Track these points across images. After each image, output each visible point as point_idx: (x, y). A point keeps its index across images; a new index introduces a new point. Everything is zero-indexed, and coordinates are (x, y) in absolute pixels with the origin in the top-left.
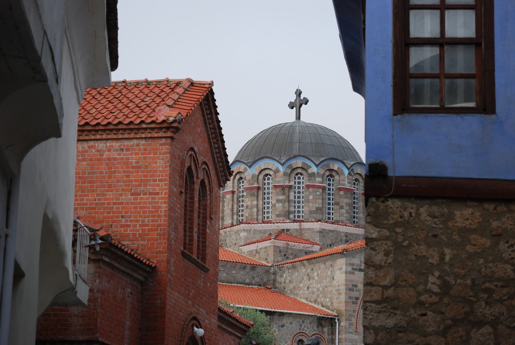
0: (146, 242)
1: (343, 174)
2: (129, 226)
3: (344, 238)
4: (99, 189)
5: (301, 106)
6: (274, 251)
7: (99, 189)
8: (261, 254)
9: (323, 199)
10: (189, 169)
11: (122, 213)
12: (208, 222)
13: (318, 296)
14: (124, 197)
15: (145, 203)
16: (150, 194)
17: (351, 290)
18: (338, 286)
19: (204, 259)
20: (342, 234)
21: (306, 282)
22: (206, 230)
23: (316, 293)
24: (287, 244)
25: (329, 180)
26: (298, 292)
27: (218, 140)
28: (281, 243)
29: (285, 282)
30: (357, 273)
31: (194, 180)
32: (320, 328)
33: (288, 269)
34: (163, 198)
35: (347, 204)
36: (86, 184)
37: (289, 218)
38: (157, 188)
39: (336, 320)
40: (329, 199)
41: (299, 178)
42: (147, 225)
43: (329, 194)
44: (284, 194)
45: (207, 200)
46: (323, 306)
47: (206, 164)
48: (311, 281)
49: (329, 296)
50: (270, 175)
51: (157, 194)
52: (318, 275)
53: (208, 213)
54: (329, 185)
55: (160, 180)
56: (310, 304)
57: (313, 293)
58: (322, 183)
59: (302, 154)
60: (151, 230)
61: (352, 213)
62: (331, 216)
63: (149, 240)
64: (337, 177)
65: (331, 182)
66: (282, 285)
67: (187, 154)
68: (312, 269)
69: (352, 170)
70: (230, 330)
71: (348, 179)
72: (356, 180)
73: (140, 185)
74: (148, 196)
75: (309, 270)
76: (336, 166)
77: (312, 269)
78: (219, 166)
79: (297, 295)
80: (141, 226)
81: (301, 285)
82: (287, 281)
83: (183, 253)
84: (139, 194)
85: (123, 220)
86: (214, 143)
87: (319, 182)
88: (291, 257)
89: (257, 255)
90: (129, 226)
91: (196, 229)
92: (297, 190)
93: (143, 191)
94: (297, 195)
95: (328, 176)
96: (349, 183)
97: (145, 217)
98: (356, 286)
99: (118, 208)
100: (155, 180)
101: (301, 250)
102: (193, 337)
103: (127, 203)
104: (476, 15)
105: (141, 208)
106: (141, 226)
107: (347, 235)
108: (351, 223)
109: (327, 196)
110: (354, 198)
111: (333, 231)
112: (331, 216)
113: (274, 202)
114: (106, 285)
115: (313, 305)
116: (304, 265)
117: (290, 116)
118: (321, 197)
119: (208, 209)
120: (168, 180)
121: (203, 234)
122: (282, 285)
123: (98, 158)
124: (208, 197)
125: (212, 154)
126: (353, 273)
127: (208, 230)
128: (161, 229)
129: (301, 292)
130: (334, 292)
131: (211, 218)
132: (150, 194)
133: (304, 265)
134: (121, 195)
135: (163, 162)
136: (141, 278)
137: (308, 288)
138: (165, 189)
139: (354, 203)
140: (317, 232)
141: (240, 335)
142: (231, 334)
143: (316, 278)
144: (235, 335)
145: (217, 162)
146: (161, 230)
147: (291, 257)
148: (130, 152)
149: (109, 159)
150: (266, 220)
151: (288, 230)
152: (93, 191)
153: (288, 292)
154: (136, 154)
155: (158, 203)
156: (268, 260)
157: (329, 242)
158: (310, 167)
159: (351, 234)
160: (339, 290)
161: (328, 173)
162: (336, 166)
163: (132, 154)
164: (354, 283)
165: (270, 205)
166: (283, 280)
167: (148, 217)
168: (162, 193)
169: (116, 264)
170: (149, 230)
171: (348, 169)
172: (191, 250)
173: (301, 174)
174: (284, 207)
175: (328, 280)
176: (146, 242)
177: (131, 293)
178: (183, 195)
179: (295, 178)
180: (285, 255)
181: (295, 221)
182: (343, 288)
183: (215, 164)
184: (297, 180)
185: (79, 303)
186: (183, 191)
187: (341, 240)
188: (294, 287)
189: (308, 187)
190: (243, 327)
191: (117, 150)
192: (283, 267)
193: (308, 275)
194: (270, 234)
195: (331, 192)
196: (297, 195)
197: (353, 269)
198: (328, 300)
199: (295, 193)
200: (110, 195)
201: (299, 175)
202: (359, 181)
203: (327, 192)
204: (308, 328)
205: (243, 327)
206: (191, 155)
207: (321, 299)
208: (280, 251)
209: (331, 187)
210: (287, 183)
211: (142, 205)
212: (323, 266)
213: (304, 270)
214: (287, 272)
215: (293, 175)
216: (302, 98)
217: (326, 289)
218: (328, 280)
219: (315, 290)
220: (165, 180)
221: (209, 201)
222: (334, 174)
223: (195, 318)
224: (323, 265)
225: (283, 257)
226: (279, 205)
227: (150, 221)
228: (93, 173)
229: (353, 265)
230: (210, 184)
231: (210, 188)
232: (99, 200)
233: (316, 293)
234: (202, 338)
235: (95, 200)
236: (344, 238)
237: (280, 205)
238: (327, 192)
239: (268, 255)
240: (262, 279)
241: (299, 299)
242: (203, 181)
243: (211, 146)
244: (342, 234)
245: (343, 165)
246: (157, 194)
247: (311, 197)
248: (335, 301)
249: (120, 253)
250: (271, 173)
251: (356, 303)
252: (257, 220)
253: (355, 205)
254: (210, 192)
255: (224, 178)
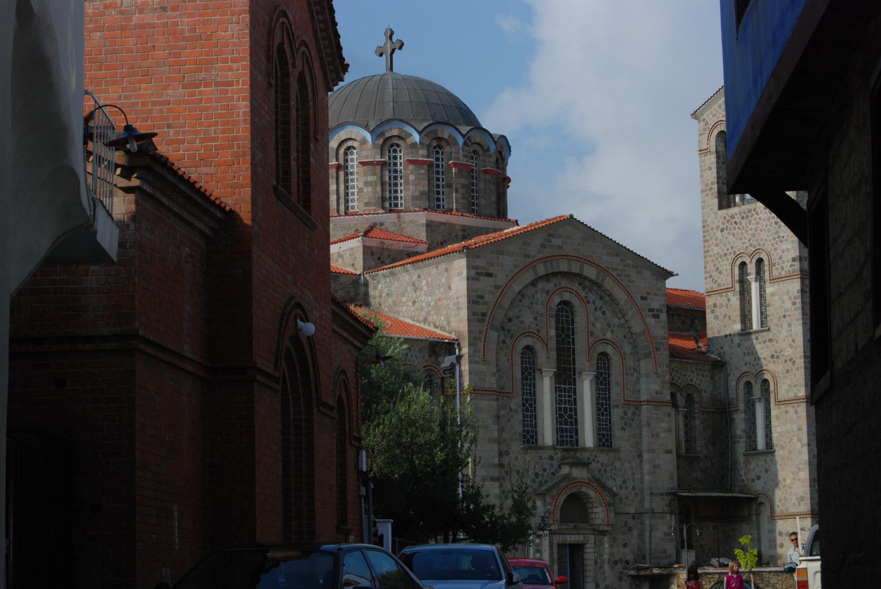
0: (212, 170)
1: (456, 143)
2: (182, 142)
3: (461, 233)
4: (125, 79)
5: (393, 51)
6: (364, 253)
7: (125, 79)
8: (345, 257)
9: (429, 180)
10: (281, 49)
11: (167, 119)
12: (312, 146)
13: (428, 313)
14: (170, 92)
15: (210, 100)
16: (217, 84)
17: (474, 302)
18: (457, 298)
19: (307, 207)
20: (458, 228)
21: (410, 295)
22: (309, 159)
23: (426, 309)
24: (381, 242)
25: (437, 153)
26: (400, 308)
27: (323, 8)
28: (373, 243)
29: (380, 296)
30: (482, 278)
31: (288, 69)
32: (433, 358)
33: (385, 277)
34: (239, 91)
35: (463, 186)
36: (103, 72)
37: (383, 208)
38: (230, 73)
39: (456, 346)
40: (438, 179)
41: (395, 151)
42: (215, 139)
43: (438, 173)
44: (374, 174)
45: (308, 109)
46: (436, 327)
47: (307, 46)
48: (418, 292)
49: (444, 312)
50: (354, 148)
51: (230, 84)
52: (427, 284)
53: (312, 131)
54: (437, 159)
55: (234, 60)
56: (418, 324)
57: (422, 309)
58: (428, 156)
59: (399, 118)
60: (222, 147)
61: (470, 199)
62: (441, 203)
63: (218, 165)
64: (447, 149)
65: (440, 156)
66: (377, 300)
67: (277, 20)
68: (419, 276)
69: (469, 138)
70: (345, 334)
71: (463, 151)
72: (475, 152)
73: (199, 70)
74: (213, 88)
75: (415, 278)
76: (446, 132)
77: (419, 276)
78: (326, 53)
79: (398, 313)
80: (202, 141)
81: (404, 299)
82: (384, 295)
83: (275, 189)
84: (197, 86)
85: (172, 131)
86: (318, 13)
87: (423, 156)
88: (387, 261)
89: (340, 260)
90: (182, 142)
91: (294, 155)
92: (392, 168)
93: (204, 79)
94: (393, 175)
95: (435, 147)
96: (465, 156)
97: (210, 126)
98: (482, 297)
99: (161, 111)
100: (225, 61)
101: (401, 251)
102: (296, 338)
103: (178, 103)
104: (329, 266)
105: (201, 109)
106: (202, 141)
107: (464, 228)
108: (469, 212)
109: (435, 176)
110: (473, 178)
111: (444, 224)
112: (441, 203)
113: (361, 185)
114: (148, 235)
115: (422, 325)
116: (407, 271)
117: (379, 66)
118: (426, 176)
119: (312, 124)
120: (248, 59)
121: (305, 166)
122: (377, 300)
123: (122, 26)
124: (311, 103)
125: (315, 31)
126: (478, 280)
127: (312, 160)
128: (238, 145)
129: (404, 308)
130: (452, 307)
131: (316, 140)
132: (217, 84)
133: (407, 271)
134: (166, 88)
135: (237, 28)
136: (208, 231)
137: (414, 303)
138: (243, 59)
139: (473, 184)
140: (422, 225)
141: (358, 344)
142: (347, 341)
143: (425, 288)
144: (352, 343)
145: (322, 47)
146: (238, 148)
147: (387, 261)
148: (178, 13)
149: (142, 26)
150: (351, 211)
151: (382, 224)
152: (114, 83)
153: (386, 309)
154: (190, 15)
155: (232, 99)
156: (356, 266)
157: (440, 239)
158: (411, 135)
159: (469, 227)
160: (458, 303)
161: (435, 143)
162: (446, 132)
163: (182, 16)
164: (479, 293)
165: (356, 190)
166: (377, 293)
167: (216, 124)
168: (238, 82)
169: (164, 200)
170: (217, 148)
171: (463, 136)
172: (287, 187)
173: (398, 146)
174: (375, 192)
175: (442, 290)
176: (212, 170)
177: (190, 256)
178: (273, 90)
179: (389, 152)
180: (379, 259)
181: (391, 211)
182: (464, 301)
183: (319, 51)
184: (392, 154)
185: (101, 256)
186: (273, 82)
187: (457, 236)
188: (394, 303)
189: (410, 162)
190: (364, 331)
191: (156, 9)
192: (377, 275)
193: (413, 284)
194: (357, 230)
195: (441, 170)
196: (393, 175)
197: (477, 274)
198: (442, 317)
199: (390, 172)
200: (146, 89)
201: (395, 147)
202: (478, 154)
203: (435, 169)
204: (417, 358)
205: (364, 331)
206: (283, 23)
207: (433, 317)
208: (372, 254)
209: (440, 163)
210: (378, 159)
211: (203, 105)
212: (434, 271)
213: (407, 278)
214: (383, 282)
215: (387, 147)
216: (394, 40)
217: (439, 303)
218: (442, 290)
219: (424, 305)
220: (243, 59)
221: (312, 111)
222: (443, 144)
223: (299, 305)
224: (435, 269)
225: (377, 262)
226: (368, 190)
227: (218, 132)
228: (114, 52)
229: (477, 267)
230: (312, 82)
231: (313, 89)
232: (126, 98)
233: (426, 309)
234: (310, 338)
235: (120, 99)
236: (461, 233)
237: (370, 189)
238: (435, 169)
239: (355, 259)
240: (348, 293)
241: (401, 319)
242: (301, 75)
243: (313, 18)
244: (458, 228)
245: (455, 131)
246: (230, 84)
247: (412, 177)
248: (453, 319)
249: (169, 176)
250: (355, 144)
251: (483, 321)
252: (338, 211)
253: (474, 188)
254: (314, 95)
255: (334, 75)
